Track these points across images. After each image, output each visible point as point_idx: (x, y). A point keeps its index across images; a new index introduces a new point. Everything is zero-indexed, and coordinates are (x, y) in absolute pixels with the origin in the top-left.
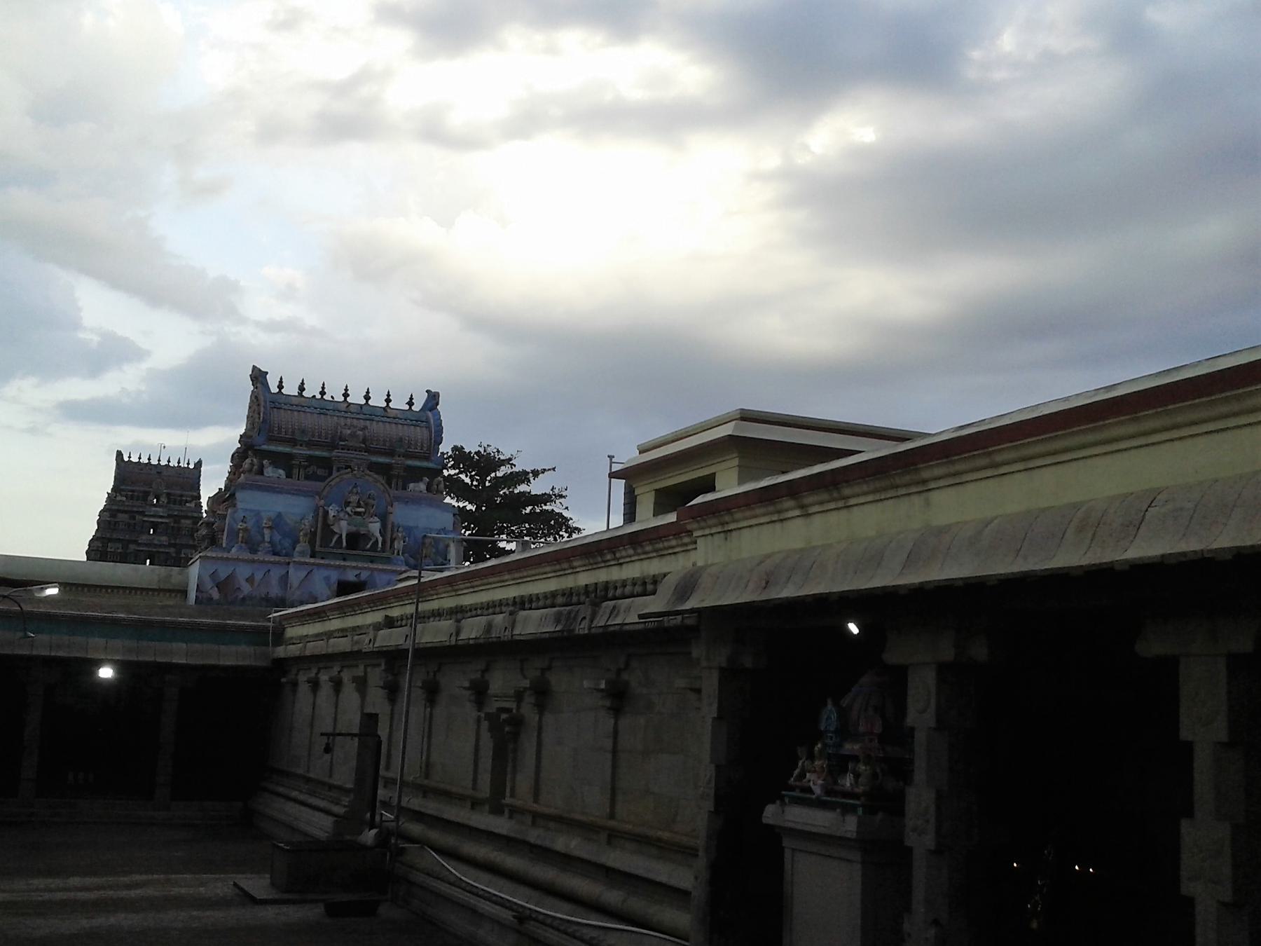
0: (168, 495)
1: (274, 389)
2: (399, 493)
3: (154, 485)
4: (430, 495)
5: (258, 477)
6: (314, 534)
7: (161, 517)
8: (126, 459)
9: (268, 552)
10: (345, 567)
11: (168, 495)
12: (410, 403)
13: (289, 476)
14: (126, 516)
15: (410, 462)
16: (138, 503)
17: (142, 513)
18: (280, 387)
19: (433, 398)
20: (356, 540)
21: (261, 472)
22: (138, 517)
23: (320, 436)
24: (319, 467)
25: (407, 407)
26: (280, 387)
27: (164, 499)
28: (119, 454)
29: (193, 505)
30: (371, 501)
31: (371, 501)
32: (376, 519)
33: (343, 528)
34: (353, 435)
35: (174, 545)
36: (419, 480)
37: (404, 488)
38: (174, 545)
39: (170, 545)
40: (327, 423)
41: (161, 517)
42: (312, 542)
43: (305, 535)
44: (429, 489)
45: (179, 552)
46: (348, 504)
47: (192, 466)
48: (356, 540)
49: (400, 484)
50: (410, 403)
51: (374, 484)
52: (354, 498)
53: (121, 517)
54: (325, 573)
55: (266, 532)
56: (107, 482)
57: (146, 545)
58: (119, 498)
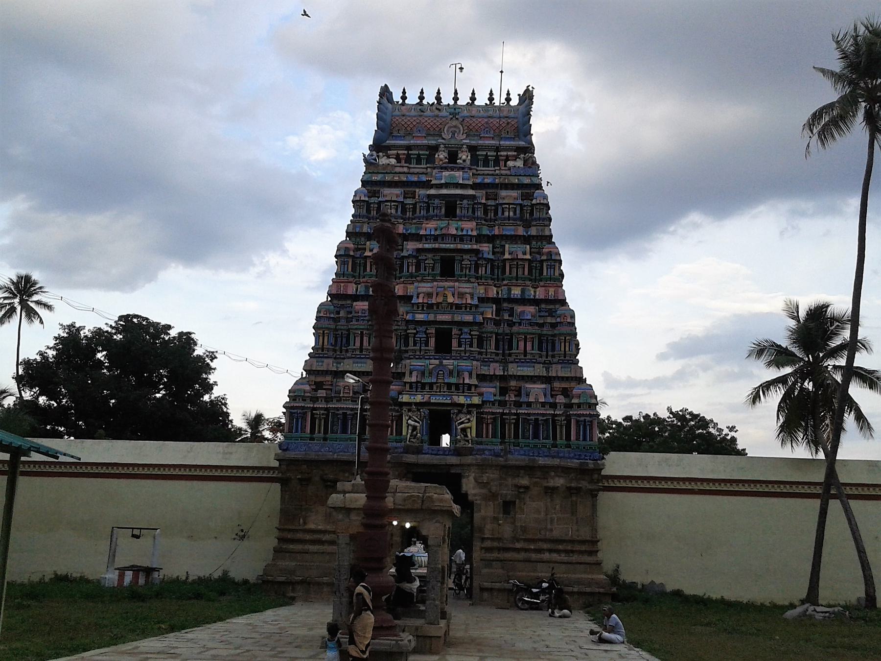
0: (472, 149)
3: (447, 135)
7: (463, 186)
8: (397, 97)
11: (472, 149)
14: (514, 193)
16: (416, 168)
17: (427, 185)
18: (404, 98)
22: (421, 192)
26: (404, 98)
27: (464, 156)
28: (385, 93)
29: (519, 163)
35: (491, 239)
38: (491, 239)
39: (480, 239)
41: (463, 186)
45: (498, 251)
47: (515, 102)
53: (392, 193)
56: (364, 129)
57: (436, 238)
58: (384, 161)
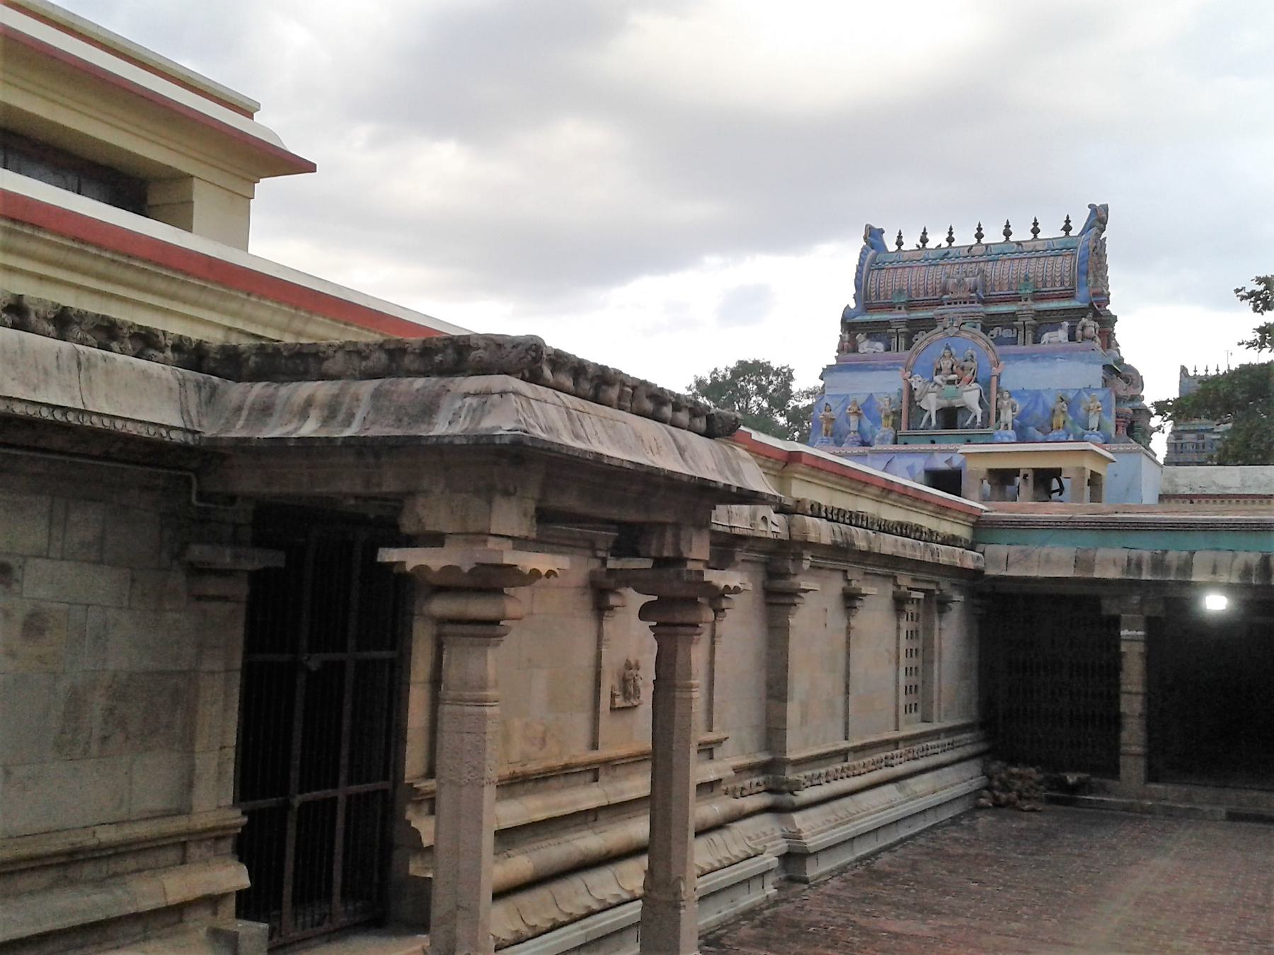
1: (892, 247)
2: (1030, 347)
4: (1074, 344)
5: (854, 355)
6: (898, 414)
9: (853, 443)
10: (932, 452)
12: (1067, 228)
13: (888, 349)
14: (1193, 436)
15: (993, 309)
18: (899, 243)
19: (1099, 217)
20: (950, 417)
21: (855, 350)
22: (1207, 436)
23: (926, 293)
24: (1004, 328)
25: (1063, 233)
30: (968, 364)
31: (968, 364)
32: (974, 385)
33: (931, 404)
34: (960, 284)
36: (1055, 327)
37: (1037, 341)
40: (934, 276)
42: (896, 425)
43: (887, 417)
44: (1072, 338)
46: (939, 371)
48: (950, 417)
49: (1030, 336)
50: (1067, 228)
51: (973, 343)
52: (946, 364)
54: (909, 461)
55: (853, 419)
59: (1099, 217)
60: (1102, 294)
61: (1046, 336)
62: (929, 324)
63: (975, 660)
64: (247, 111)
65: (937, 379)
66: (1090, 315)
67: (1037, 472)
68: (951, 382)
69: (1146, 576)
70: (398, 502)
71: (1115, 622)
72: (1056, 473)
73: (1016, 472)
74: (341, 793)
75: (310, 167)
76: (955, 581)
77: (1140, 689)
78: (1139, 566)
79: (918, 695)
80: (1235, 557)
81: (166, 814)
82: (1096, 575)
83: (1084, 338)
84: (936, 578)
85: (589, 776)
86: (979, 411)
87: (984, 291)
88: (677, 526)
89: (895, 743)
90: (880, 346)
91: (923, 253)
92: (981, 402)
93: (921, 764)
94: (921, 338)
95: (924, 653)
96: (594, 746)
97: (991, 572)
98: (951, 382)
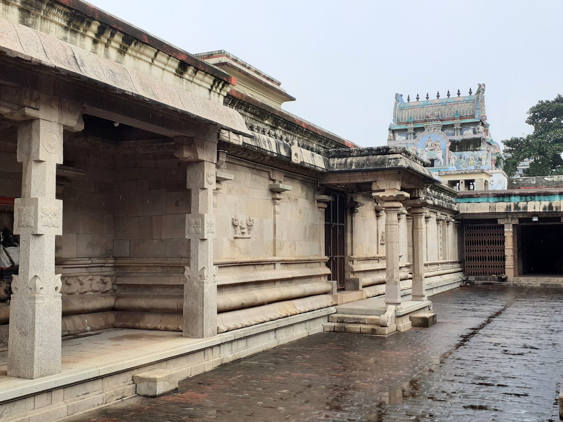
1: (406, 101)
12: (470, 93)
13: (407, 139)
18: (409, 100)
30: (438, 143)
31: (438, 143)
32: (440, 151)
34: (432, 114)
40: (423, 113)
50: (470, 93)
52: (429, 144)
59: (481, 90)
60: (484, 116)
61: (465, 132)
62: (422, 129)
63: (457, 241)
64: (279, 84)
65: (426, 149)
66: (481, 124)
67: (466, 181)
68: (432, 150)
69: (512, 211)
70: (370, 184)
71: (502, 227)
72: (473, 181)
73: (458, 181)
74: (338, 257)
75: (292, 99)
76: (451, 215)
77: (512, 247)
78: (510, 207)
79: (443, 250)
80: (541, 203)
81: (317, 255)
82: (497, 211)
83: (479, 132)
84: (446, 214)
85: (377, 261)
86: (442, 160)
87: (441, 116)
88: (418, 189)
89: (438, 264)
90: (404, 138)
91: (418, 103)
92: (443, 157)
93: (445, 271)
94: (419, 134)
95: (444, 238)
96: (378, 253)
97: (461, 212)
98: (432, 150)
